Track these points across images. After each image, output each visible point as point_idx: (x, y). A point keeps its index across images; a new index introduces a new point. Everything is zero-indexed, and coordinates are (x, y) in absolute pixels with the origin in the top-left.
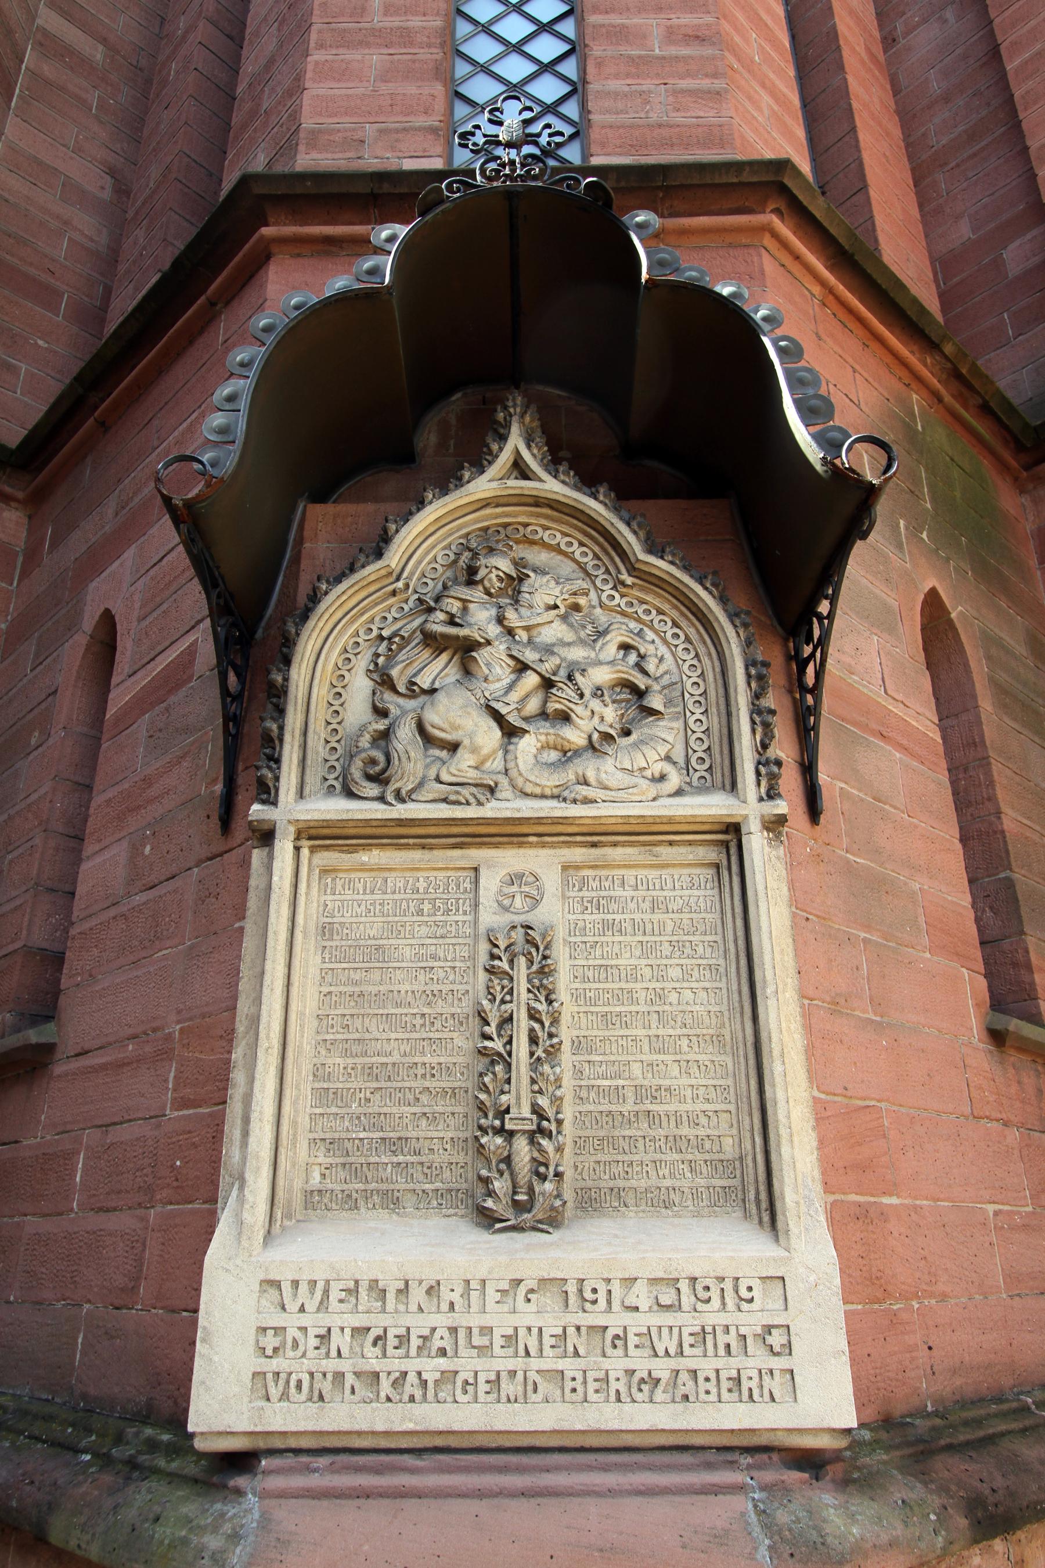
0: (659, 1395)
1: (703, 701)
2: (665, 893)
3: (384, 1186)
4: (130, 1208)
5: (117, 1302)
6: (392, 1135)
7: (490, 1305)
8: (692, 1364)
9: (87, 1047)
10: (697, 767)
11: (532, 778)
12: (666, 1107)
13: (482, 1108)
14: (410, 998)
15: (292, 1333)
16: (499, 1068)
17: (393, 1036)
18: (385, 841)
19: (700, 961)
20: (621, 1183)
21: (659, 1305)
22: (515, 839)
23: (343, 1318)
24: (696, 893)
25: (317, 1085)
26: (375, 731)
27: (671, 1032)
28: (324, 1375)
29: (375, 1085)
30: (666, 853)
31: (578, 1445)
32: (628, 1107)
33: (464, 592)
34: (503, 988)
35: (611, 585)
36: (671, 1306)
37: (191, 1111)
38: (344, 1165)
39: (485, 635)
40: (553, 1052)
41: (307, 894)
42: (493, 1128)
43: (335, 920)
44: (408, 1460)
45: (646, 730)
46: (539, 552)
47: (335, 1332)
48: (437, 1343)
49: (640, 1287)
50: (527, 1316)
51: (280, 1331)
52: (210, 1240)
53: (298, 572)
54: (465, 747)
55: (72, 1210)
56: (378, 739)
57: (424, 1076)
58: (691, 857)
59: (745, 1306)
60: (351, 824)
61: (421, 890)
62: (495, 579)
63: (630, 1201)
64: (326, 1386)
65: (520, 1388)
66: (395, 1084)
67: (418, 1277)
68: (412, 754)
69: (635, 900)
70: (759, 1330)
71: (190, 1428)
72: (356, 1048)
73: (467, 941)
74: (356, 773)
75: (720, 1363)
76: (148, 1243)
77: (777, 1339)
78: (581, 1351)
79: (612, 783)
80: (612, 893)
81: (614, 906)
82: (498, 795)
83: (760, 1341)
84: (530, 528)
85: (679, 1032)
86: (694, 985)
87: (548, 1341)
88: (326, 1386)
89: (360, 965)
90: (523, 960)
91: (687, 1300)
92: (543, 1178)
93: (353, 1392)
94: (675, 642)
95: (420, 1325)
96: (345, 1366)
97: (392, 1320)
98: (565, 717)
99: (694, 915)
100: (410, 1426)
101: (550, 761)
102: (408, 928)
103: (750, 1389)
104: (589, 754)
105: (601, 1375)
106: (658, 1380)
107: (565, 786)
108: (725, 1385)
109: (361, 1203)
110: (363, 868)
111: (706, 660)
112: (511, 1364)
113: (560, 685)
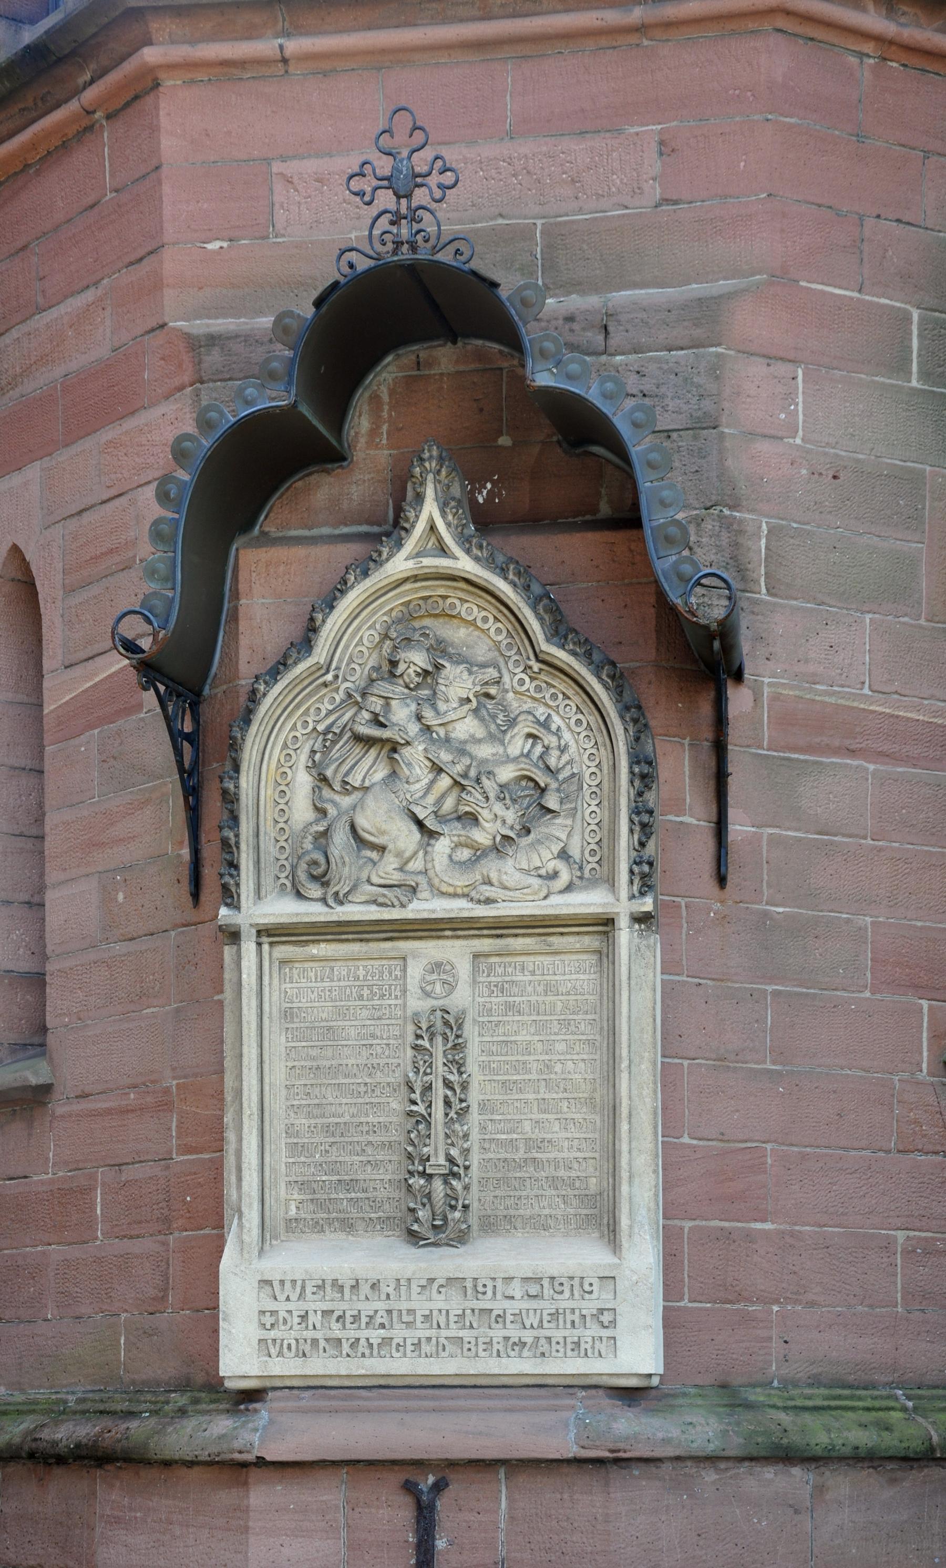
0: (526, 1353)
1: (598, 792)
2: (557, 978)
3: (342, 1216)
4: (151, 1235)
5: (151, 1309)
6: (346, 1178)
7: (414, 1296)
8: (548, 1333)
9: (88, 1089)
10: (590, 859)
11: (446, 879)
12: (548, 1155)
13: (410, 1157)
14: (355, 1070)
15: (282, 1314)
16: (421, 1127)
17: (344, 1101)
18: (329, 937)
19: (581, 1037)
20: (512, 1212)
21: (529, 1296)
22: (434, 934)
23: (315, 1305)
24: (582, 977)
25: (289, 1141)
26: (317, 832)
27: (555, 1096)
28: (306, 1340)
29: (332, 1140)
30: (557, 942)
31: (473, 1384)
32: (521, 1154)
33: (383, 688)
34: (425, 1062)
35: (521, 668)
36: (536, 1296)
37: (194, 1157)
38: (312, 1200)
39: (405, 736)
40: (463, 1113)
41: (270, 984)
42: (419, 1173)
43: (294, 1005)
44: (363, 1393)
45: (544, 830)
46: (458, 628)
47: (311, 1313)
48: (379, 1320)
49: (516, 1284)
50: (439, 1303)
51: (273, 1313)
52: (221, 1257)
53: (237, 634)
54: (390, 851)
55: (97, 1238)
56: (319, 838)
57: (367, 1133)
58: (578, 946)
59: (587, 1296)
60: (301, 926)
61: (361, 978)
62: (413, 675)
63: (519, 1225)
64: (307, 1348)
65: (434, 1348)
66: (347, 1139)
67: (364, 1277)
68: (347, 859)
69: (532, 984)
70: (595, 1312)
71: (221, 1374)
72: (316, 1111)
73: (399, 1022)
74: (302, 876)
75: (567, 1333)
76: (171, 1262)
77: (606, 1318)
78: (475, 1325)
79: (510, 884)
80: (514, 978)
81: (515, 990)
82: (420, 895)
83: (595, 1320)
84: (449, 601)
85: (561, 1095)
86: (575, 1057)
87: (452, 1319)
88: (307, 1348)
89: (317, 1043)
90: (439, 1039)
91: (548, 1292)
92: (453, 1208)
93: (325, 1351)
94: (578, 730)
95: (367, 1308)
96: (319, 1335)
97: (349, 1306)
98: (472, 819)
99: (579, 997)
100: (363, 1372)
101: (463, 860)
102: (352, 1011)
103: (586, 1349)
104: (493, 855)
105: (488, 1340)
106: (525, 1343)
107: (472, 886)
108: (569, 1346)
109: (326, 1227)
110: (314, 959)
111: (602, 749)
112: (428, 1333)
113: (469, 788)
